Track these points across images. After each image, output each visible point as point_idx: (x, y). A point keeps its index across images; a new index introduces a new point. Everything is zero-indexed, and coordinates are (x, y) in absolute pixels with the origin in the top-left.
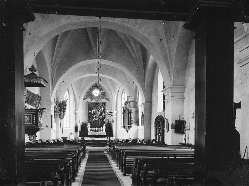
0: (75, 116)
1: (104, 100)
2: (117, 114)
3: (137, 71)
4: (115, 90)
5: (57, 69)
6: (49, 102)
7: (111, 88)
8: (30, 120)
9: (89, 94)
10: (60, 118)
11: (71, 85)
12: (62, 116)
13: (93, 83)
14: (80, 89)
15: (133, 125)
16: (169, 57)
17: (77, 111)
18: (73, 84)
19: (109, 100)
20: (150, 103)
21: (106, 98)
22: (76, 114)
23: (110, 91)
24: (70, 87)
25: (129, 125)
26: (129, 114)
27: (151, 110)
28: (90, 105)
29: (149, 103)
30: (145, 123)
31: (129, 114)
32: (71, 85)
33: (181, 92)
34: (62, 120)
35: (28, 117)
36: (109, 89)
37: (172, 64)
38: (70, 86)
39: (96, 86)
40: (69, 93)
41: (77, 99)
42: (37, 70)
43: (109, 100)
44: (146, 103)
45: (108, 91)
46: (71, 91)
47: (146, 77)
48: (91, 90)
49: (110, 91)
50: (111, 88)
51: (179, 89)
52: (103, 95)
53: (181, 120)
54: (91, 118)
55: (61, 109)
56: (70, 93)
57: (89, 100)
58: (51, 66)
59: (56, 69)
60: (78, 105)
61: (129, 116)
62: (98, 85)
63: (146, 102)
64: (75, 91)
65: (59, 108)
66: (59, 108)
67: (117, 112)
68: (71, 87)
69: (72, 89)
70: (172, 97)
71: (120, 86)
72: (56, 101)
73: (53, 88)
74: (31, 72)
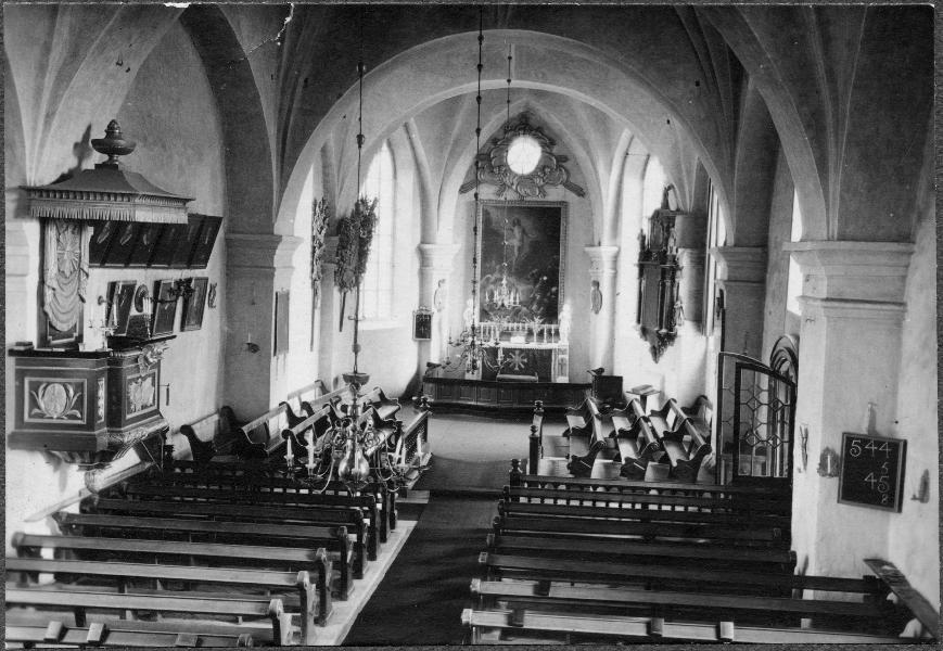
0: (417, 265)
1: (555, 194)
2: (616, 259)
3: (698, 84)
4: (609, 147)
5: (306, 81)
6: (266, 237)
7: (593, 137)
8: (35, 387)
9: (489, 162)
10: (343, 286)
11: (406, 127)
12: (349, 275)
13: (516, 109)
14: (445, 147)
15: (685, 328)
16: (821, 71)
17: (426, 247)
18: (412, 121)
19: (580, 192)
20: (759, 250)
21: (568, 185)
22: (423, 256)
23: (588, 153)
24: (400, 134)
25: (664, 331)
26: (663, 278)
27: (762, 282)
28: (494, 215)
29: (754, 250)
30: (727, 339)
31: (663, 278)
32: (406, 127)
33: (885, 272)
34: (351, 296)
35: (67, 391)
36: (585, 144)
37: (838, 123)
38: (401, 130)
39: (523, 125)
40: (394, 160)
41: (433, 189)
42: (136, 141)
43: (580, 192)
44: (737, 249)
45: (580, 153)
46: (405, 154)
47: (743, 123)
48: (500, 142)
49: (588, 153)
50: (593, 137)
51: (871, 259)
52: (557, 163)
53: (882, 429)
54: (493, 278)
55: (343, 246)
56: (398, 163)
57: (487, 192)
58: (279, 71)
59: (301, 80)
60: (435, 221)
61: (664, 285)
62: (532, 122)
63: (735, 246)
64: (421, 151)
65: (336, 239)
66: (336, 239)
67: (619, 252)
68: (405, 136)
69: (408, 147)
70: (829, 304)
71: (632, 139)
72: (324, 207)
73: (287, 168)
74: (106, 158)
